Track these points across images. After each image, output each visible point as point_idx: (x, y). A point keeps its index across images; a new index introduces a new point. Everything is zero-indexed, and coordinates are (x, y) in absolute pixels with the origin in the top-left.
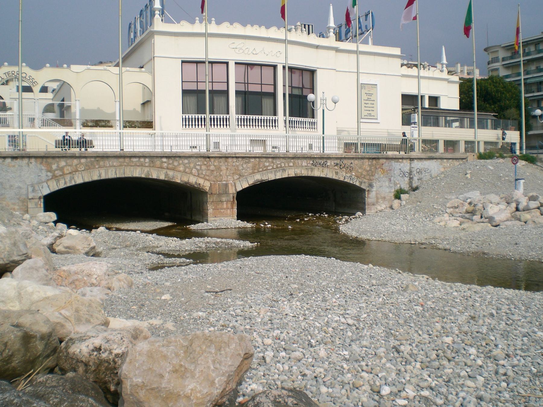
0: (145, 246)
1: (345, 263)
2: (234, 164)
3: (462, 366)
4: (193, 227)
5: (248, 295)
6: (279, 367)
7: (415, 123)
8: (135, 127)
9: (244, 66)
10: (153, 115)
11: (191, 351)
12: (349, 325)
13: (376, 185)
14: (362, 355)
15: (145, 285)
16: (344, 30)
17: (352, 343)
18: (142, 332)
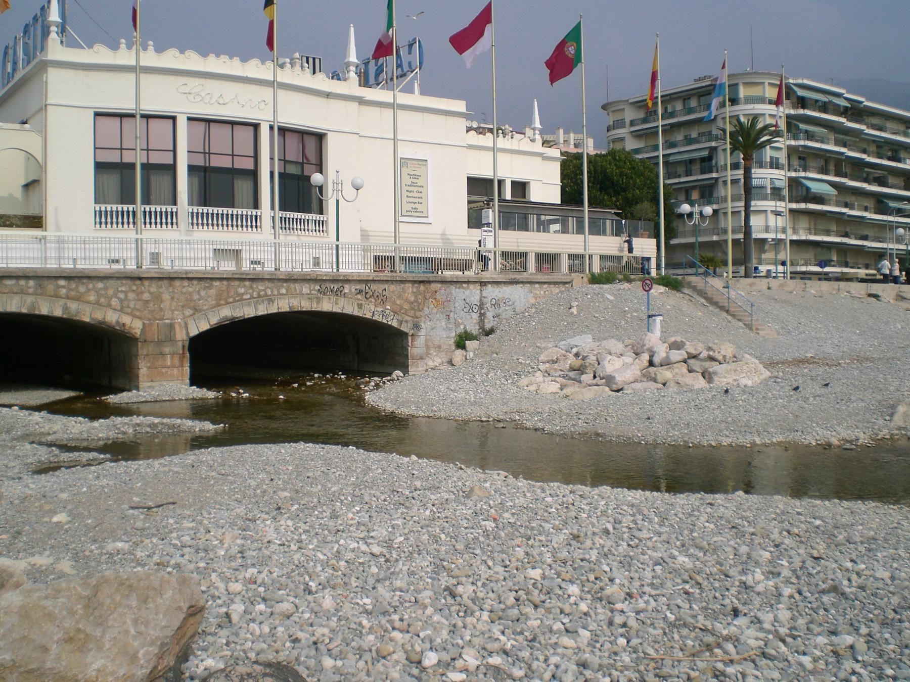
0: (28, 432)
1: (372, 454)
2: (184, 290)
3: (556, 614)
4: (112, 399)
5: (203, 512)
6: (254, 630)
7: (488, 224)
8: (11, 226)
9: (203, 124)
10: (43, 204)
11: (96, 605)
12: (373, 554)
13: (425, 325)
14: (393, 604)
15: (24, 499)
16: (372, 68)
17: (379, 585)
18: (11, 575)
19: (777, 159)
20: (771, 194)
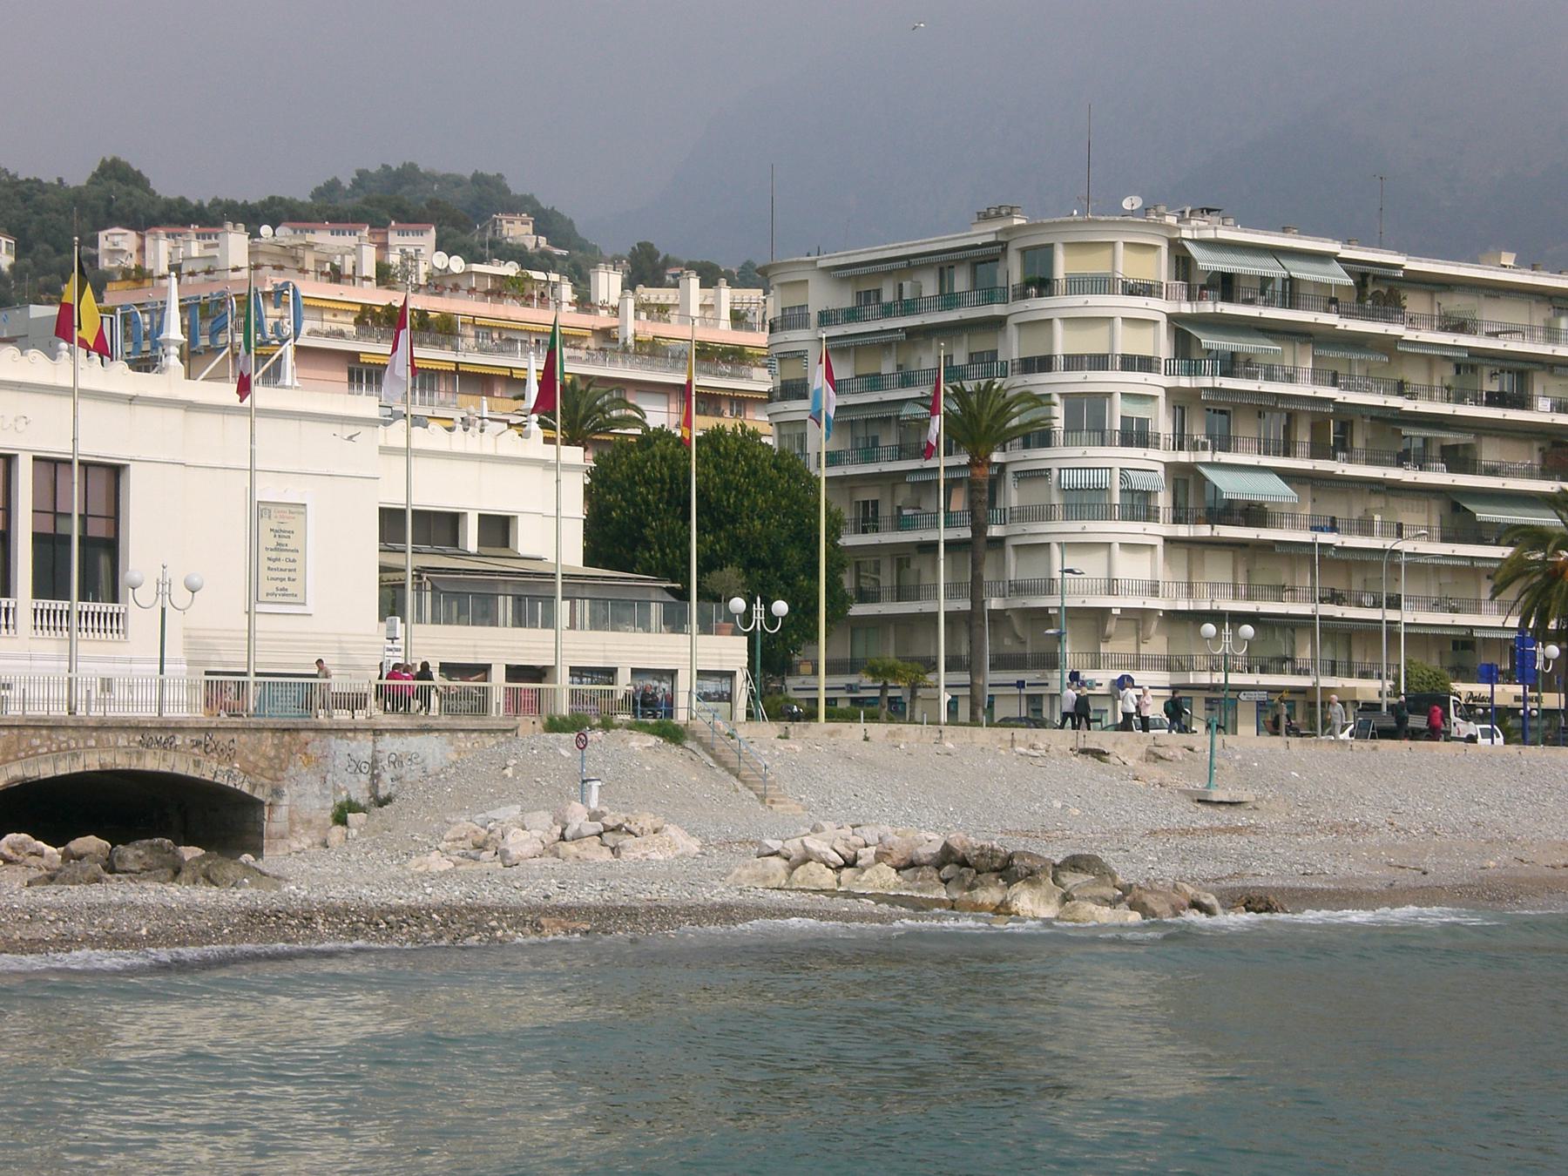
19: (1143, 422)
20: (1121, 506)
